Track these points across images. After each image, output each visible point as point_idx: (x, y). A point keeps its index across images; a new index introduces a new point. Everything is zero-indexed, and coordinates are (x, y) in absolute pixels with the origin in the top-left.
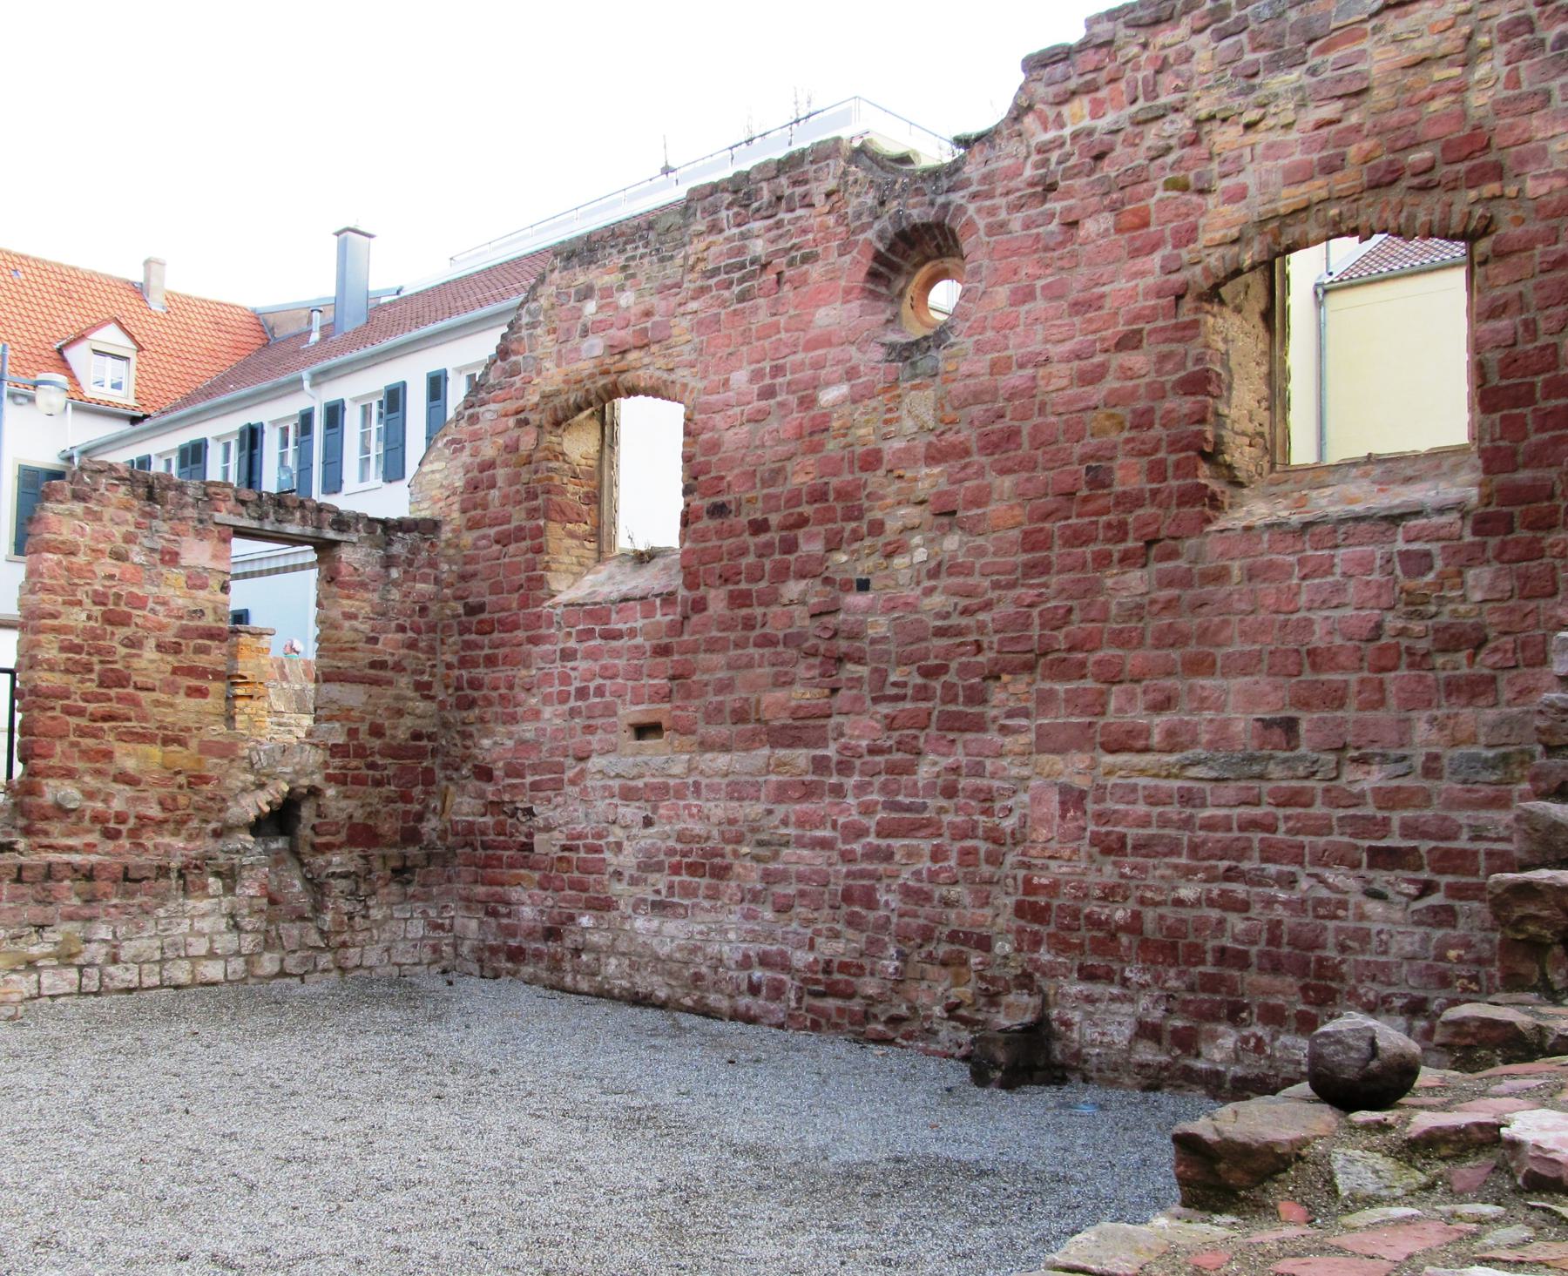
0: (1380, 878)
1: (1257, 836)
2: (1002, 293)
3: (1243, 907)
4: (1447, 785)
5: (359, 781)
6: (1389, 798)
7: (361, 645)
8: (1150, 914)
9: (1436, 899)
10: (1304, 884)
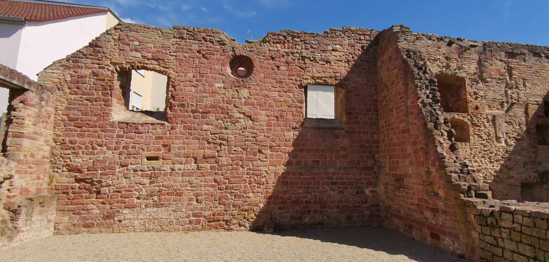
0: (333, 187)
1: (312, 181)
3: (310, 193)
4: (342, 171)
5: (26, 173)
6: (334, 174)
7: (31, 126)
8: (293, 196)
9: (341, 189)
10: (320, 189)
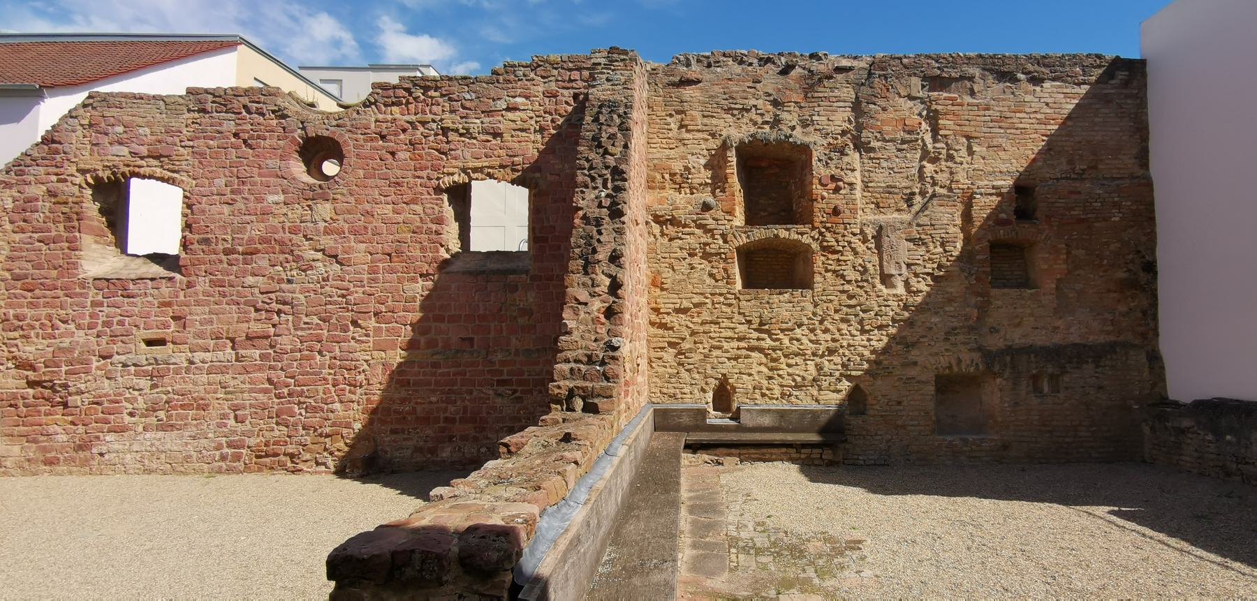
2: (361, 172)
